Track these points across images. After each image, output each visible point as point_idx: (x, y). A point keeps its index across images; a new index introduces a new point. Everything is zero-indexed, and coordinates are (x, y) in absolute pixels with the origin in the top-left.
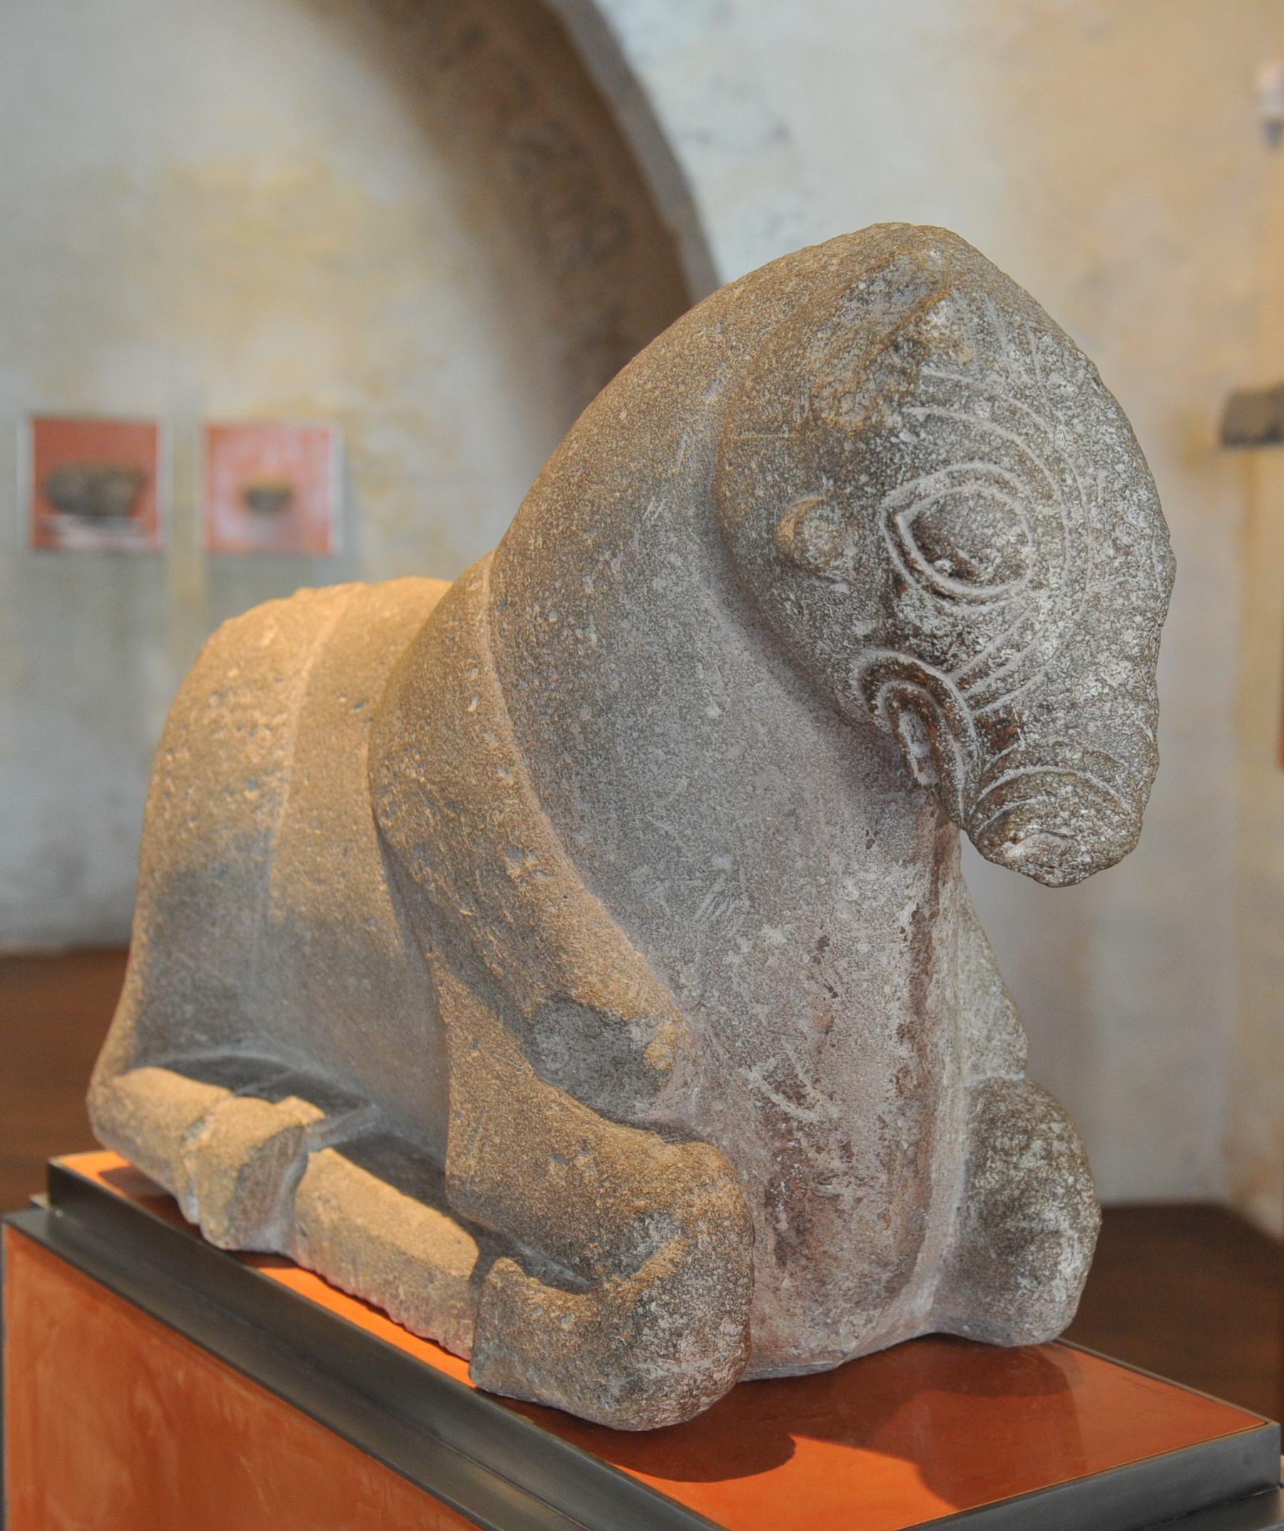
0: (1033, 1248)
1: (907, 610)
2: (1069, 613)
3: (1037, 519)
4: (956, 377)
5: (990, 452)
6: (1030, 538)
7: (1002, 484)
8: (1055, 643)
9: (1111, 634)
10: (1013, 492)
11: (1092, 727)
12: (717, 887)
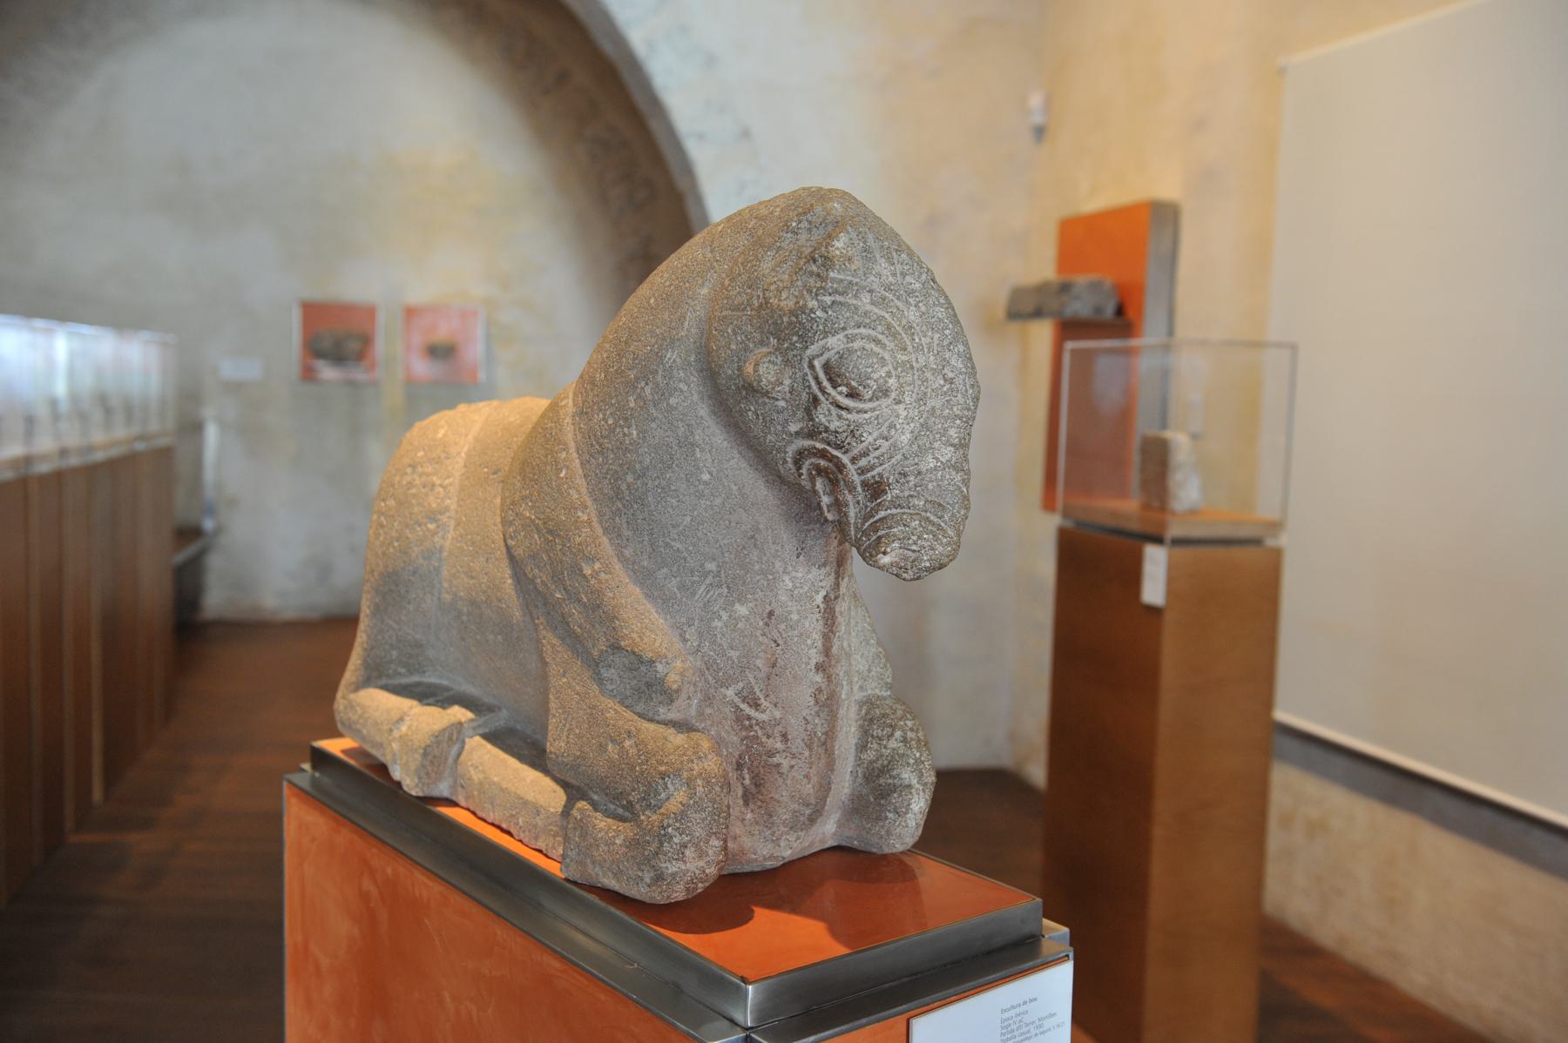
1: (821, 416)
7: (877, 342)
10: (884, 346)
12: (708, 581)
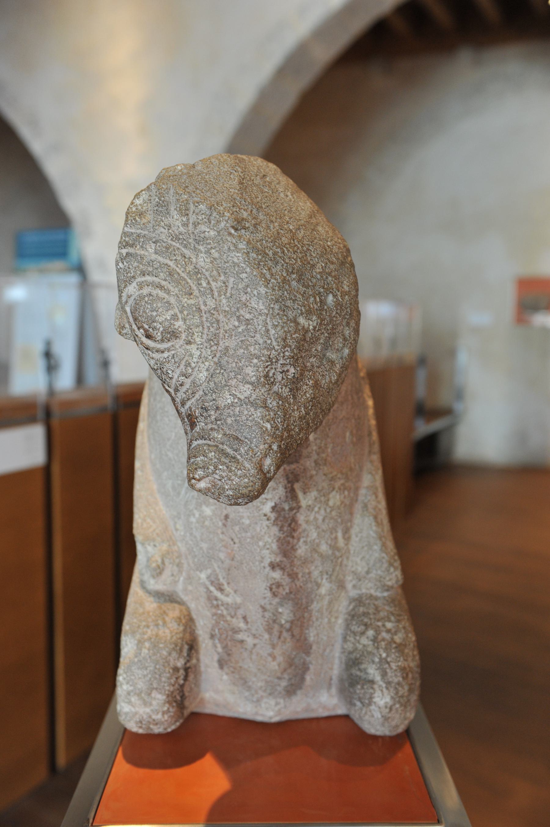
0: (359, 687)
2: (210, 357)
3: (183, 306)
4: (139, 231)
5: (153, 271)
6: (180, 316)
7: (161, 287)
8: (205, 374)
9: (236, 370)
10: (168, 292)
11: (229, 421)
